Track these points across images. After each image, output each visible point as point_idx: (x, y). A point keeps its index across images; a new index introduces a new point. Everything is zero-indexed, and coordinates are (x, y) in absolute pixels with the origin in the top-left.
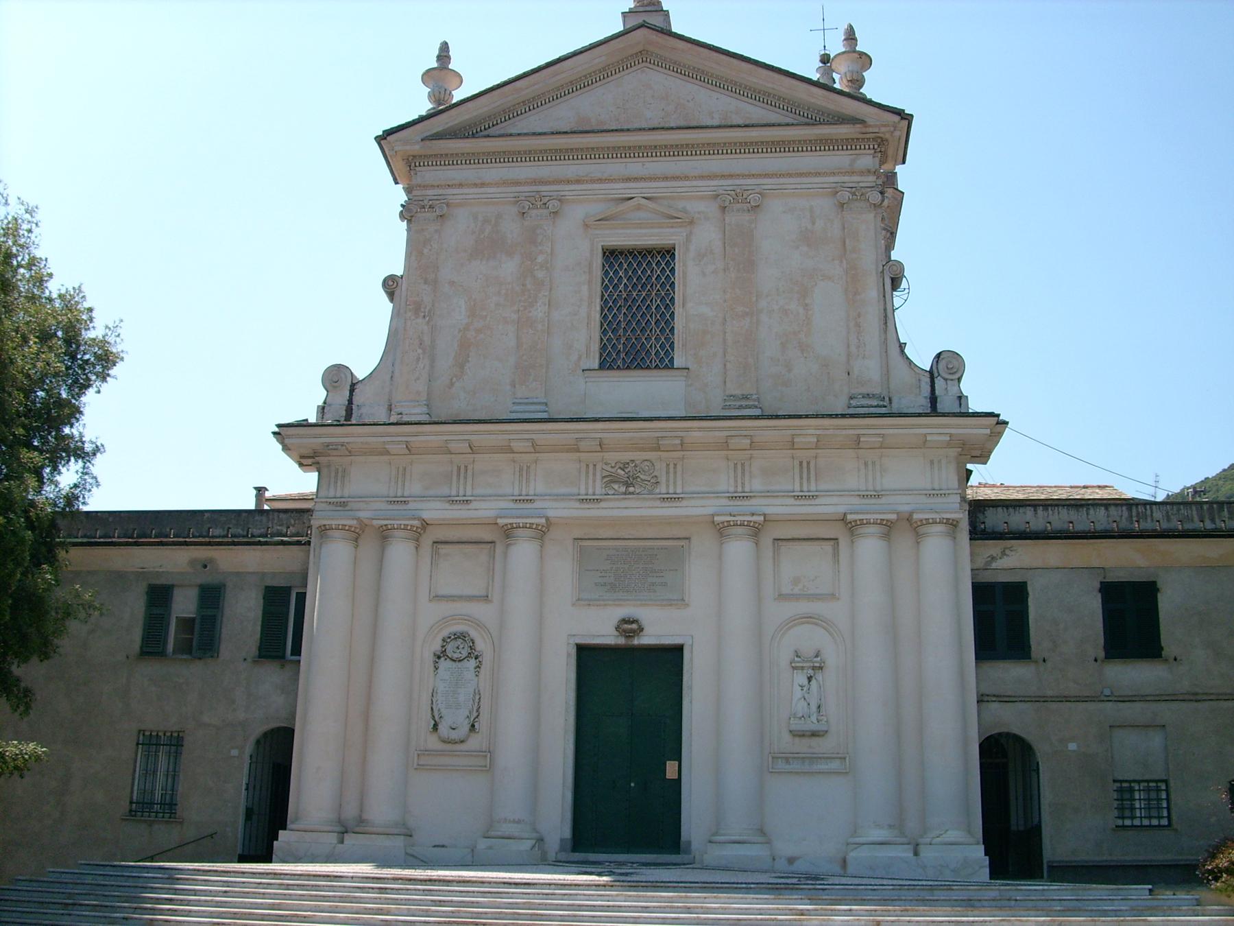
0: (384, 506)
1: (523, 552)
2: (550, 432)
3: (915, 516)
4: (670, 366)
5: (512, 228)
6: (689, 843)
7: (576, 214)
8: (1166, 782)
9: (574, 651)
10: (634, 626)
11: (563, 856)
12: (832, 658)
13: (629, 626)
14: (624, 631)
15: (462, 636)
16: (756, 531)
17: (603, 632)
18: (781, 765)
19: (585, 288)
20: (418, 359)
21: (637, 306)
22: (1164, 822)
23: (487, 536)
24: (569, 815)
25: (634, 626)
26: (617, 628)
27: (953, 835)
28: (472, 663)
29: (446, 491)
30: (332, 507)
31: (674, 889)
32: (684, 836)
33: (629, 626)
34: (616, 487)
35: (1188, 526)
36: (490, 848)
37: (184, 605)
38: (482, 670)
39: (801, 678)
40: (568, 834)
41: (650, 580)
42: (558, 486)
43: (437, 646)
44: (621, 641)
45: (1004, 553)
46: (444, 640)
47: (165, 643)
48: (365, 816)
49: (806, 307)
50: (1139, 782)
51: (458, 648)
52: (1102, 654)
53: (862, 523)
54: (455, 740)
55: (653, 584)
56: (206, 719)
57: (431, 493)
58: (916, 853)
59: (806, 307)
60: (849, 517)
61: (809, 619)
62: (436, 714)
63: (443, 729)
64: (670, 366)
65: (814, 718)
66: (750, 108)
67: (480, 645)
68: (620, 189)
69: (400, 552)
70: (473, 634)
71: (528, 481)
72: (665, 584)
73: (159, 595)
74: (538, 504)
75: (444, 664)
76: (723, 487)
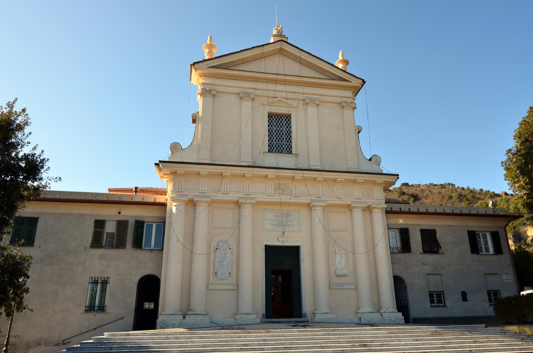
6: (306, 314)
8: (442, 292)
11: (263, 320)
21: (280, 133)
22: (443, 304)
24: (264, 305)
27: (391, 310)
31: (228, 329)
32: (304, 312)
37: (110, 228)
40: (264, 312)
47: (102, 242)
50: (435, 292)
52: (422, 252)
55: (289, 225)
58: (382, 316)
63: (219, 274)
72: (293, 225)
73: (100, 224)
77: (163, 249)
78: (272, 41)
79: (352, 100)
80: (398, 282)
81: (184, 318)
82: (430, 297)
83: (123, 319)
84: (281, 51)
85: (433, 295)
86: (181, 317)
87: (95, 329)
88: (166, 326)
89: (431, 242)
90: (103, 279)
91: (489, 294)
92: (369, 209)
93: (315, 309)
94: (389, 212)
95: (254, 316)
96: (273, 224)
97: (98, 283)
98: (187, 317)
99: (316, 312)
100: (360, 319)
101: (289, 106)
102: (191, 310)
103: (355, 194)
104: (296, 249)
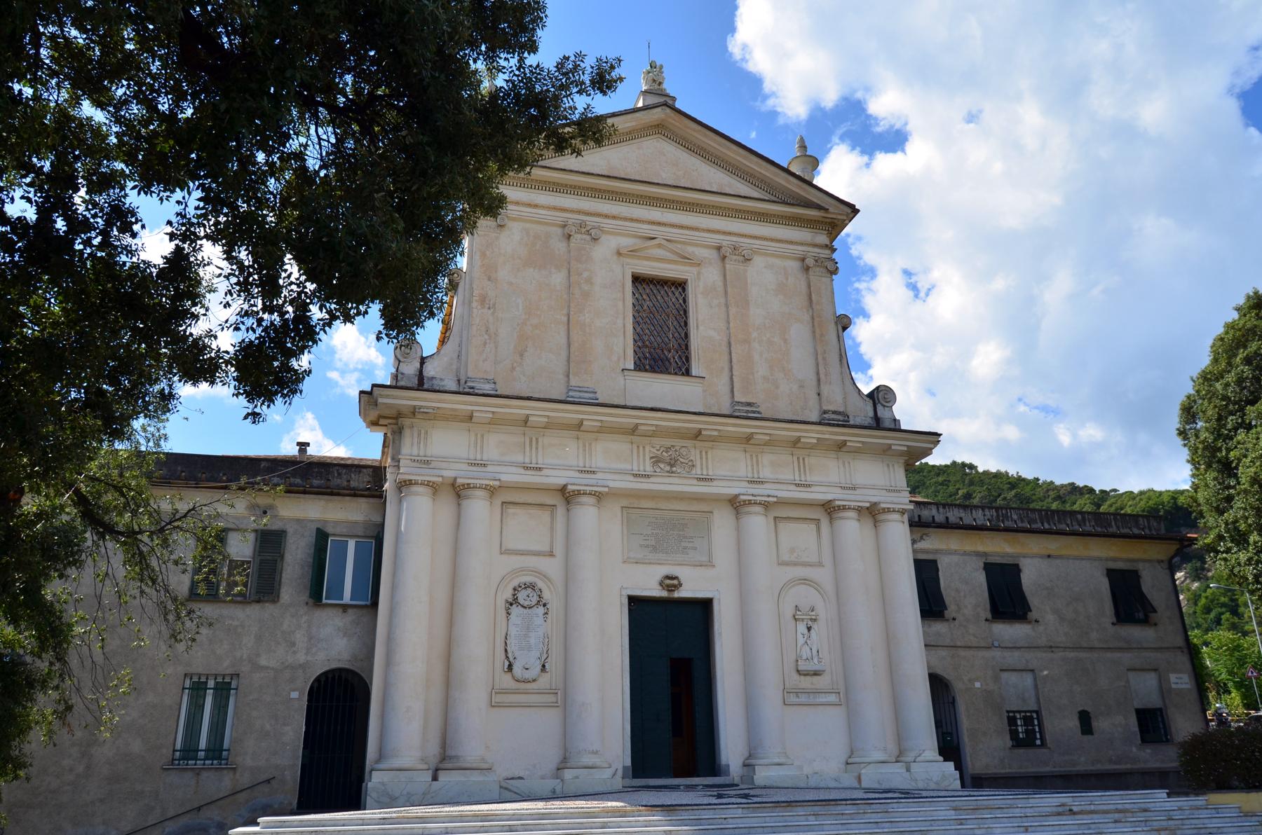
0: (465, 467)
1: (587, 514)
2: (563, 411)
3: (570, 487)
4: (687, 373)
5: (559, 246)
6: (728, 766)
7: (609, 244)
8: (1037, 712)
9: (626, 601)
10: (675, 582)
12: (821, 612)
13: (671, 582)
14: (668, 586)
15: (532, 586)
16: (492, 491)
17: (651, 588)
18: (793, 699)
19: (620, 304)
20: (485, 344)
23: (549, 500)
25: (675, 582)
26: (661, 584)
28: (541, 610)
29: (520, 458)
30: (415, 464)
33: (671, 582)
34: (662, 466)
35: (1034, 526)
36: (577, 777)
37: (241, 548)
38: (549, 616)
39: (802, 628)
40: (628, 762)
41: (683, 544)
42: (614, 463)
43: (508, 594)
44: (664, 594)
45: (922, 538)
46: (515, 589)
48: (450, 752)
49: (785, 341)
50: (1019, 712)
51: (523, 597)
52: (989, 616)
53: (579, 493)
54: (539, 682)
55: (685, 548)
56: (263, 662)
57: (507, 458)
58: (908, 770)
59: (785, 341)
60: (460, 481)
61: (805, 581)
62: (510, 655)
63: (517, 669)
64: (687, 373)
65: (816, 661)
66: (739, 185)
67: (547, 595)
68: (646, 229)
69: (479, 509)
70: (540, 584)
71: (591, 455)
72: (695, 549)
74: (490, 468)
75: (515, 610)
76: (574, 463)
77: (375, 604)
78: (640, 104)
79: (828, 252)
80: (939, 686)
81: (435, 778)
82: (1010, 725)
83: (273, 782)
84: (659, 129)
85: (1015, 719)
86: (428, 776)
87: (199, 809)
88: (390, 801)
89: (1006, 596)
90: (195, 679)
91: (1012, 721)
92: (873, 513)
93: (750, 756)
94: (918, 524)
95: (607, 774)
96: (647, 546)
97: (206, 689)
98: (443, 776)
99: (753, 761)
100: (859, 779)
101: (686, 259)
102: (451, 758)
103: (829, 477)
104: (704, 607)
